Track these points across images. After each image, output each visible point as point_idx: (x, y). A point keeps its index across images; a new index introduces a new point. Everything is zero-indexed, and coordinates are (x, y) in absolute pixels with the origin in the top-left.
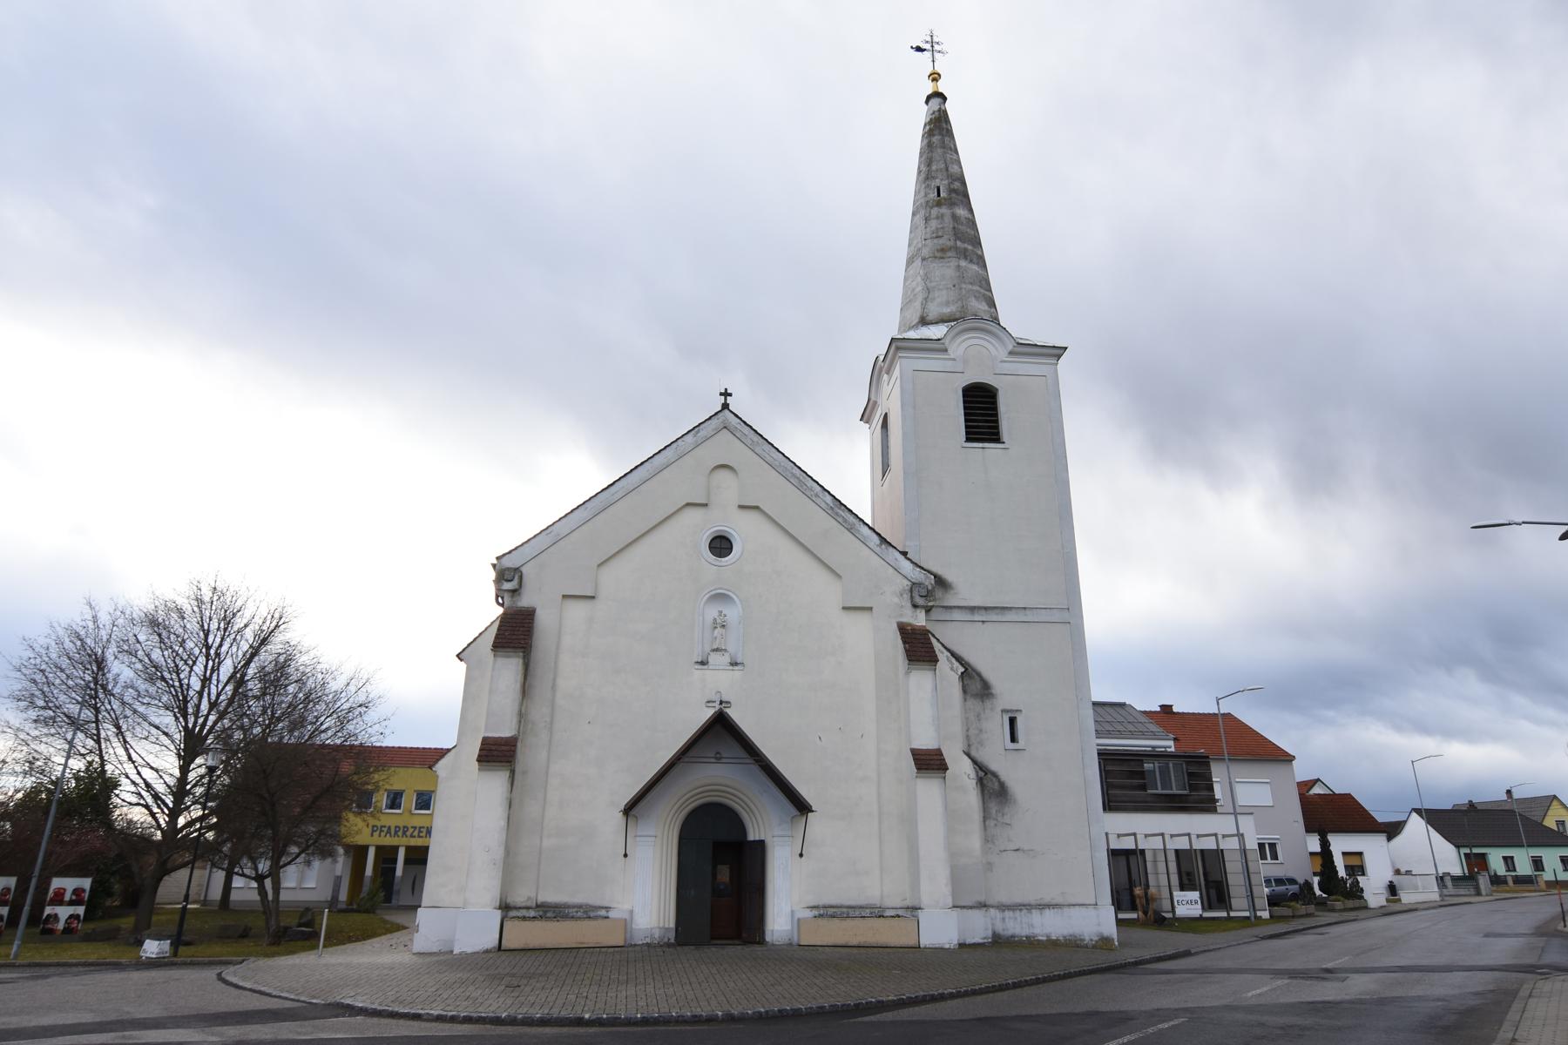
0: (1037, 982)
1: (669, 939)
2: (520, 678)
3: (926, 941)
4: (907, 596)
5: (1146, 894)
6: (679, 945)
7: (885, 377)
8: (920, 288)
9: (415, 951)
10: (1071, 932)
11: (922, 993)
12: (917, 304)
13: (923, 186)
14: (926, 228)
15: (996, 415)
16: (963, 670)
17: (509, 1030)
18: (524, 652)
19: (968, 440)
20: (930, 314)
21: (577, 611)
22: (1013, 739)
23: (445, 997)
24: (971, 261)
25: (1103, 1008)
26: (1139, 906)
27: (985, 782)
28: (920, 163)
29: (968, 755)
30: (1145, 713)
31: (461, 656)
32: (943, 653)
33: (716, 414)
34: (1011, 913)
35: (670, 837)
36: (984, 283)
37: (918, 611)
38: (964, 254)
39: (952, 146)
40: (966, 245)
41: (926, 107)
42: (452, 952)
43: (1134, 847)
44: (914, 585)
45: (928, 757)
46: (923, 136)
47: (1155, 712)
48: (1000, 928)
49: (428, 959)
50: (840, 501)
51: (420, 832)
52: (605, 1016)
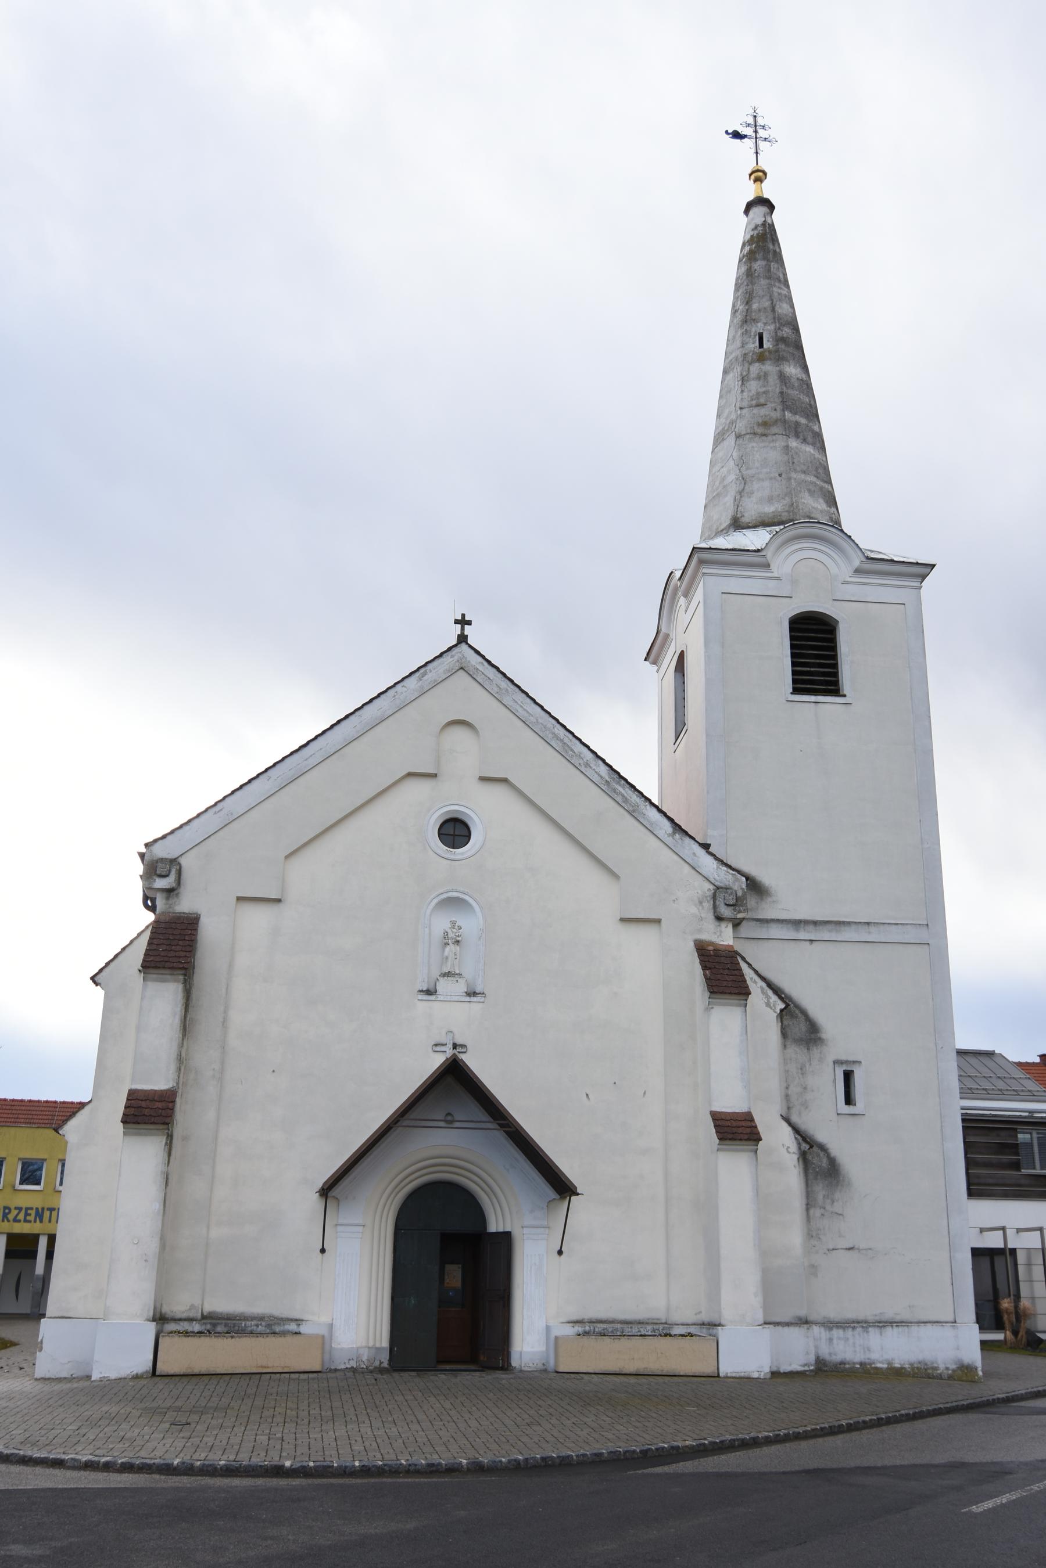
0: (879, 1423)
1: (381, 1363)
2: (179, 1009)
3: (727, 1368)
4: (708, 905)
5: (1016, 1307)
6: (395, 1370)
7: (682, 601)
8: (732, 477)
9: (39, 1373)
10: (921, 1358)
11: (729, 1437)
12: (729, 500)
13: (740, 332)
14: (742, 391)
15: (835, 657)
16: (783, 1006)
17: (185, 1481)
18: (185, 975)
19: (796, 691)
20: (746, 515)
21: (257, 918)
22: (849, 1100)
23: (92, 1438)
24: (805, 441)
25: (970, 1458)
26: (1007, 1325)
27: (810, 1158)
28: (735, 299)
29: (787, 1120)
30: (1020, 1064)
31: (97, 979)
32: (755, 982)
33: (450, 649)
34: (841, 1331)
35: (383, 1224)
36: (821, 471)
37: (723, 925)
38: (795, 431)
39: (781, 276)
40: (798, 418)
41: (744, 219)
42: (89, 1377)
43: (1002, 1246)
44: (719, 890)
45: (734, 1124)
46: (740, 261)
47: (1034, 1064)
48: (825, 1352)
49: (58, 1387)
50: (618, 773)
51: (27, 1214)
52: (311, 1464)
